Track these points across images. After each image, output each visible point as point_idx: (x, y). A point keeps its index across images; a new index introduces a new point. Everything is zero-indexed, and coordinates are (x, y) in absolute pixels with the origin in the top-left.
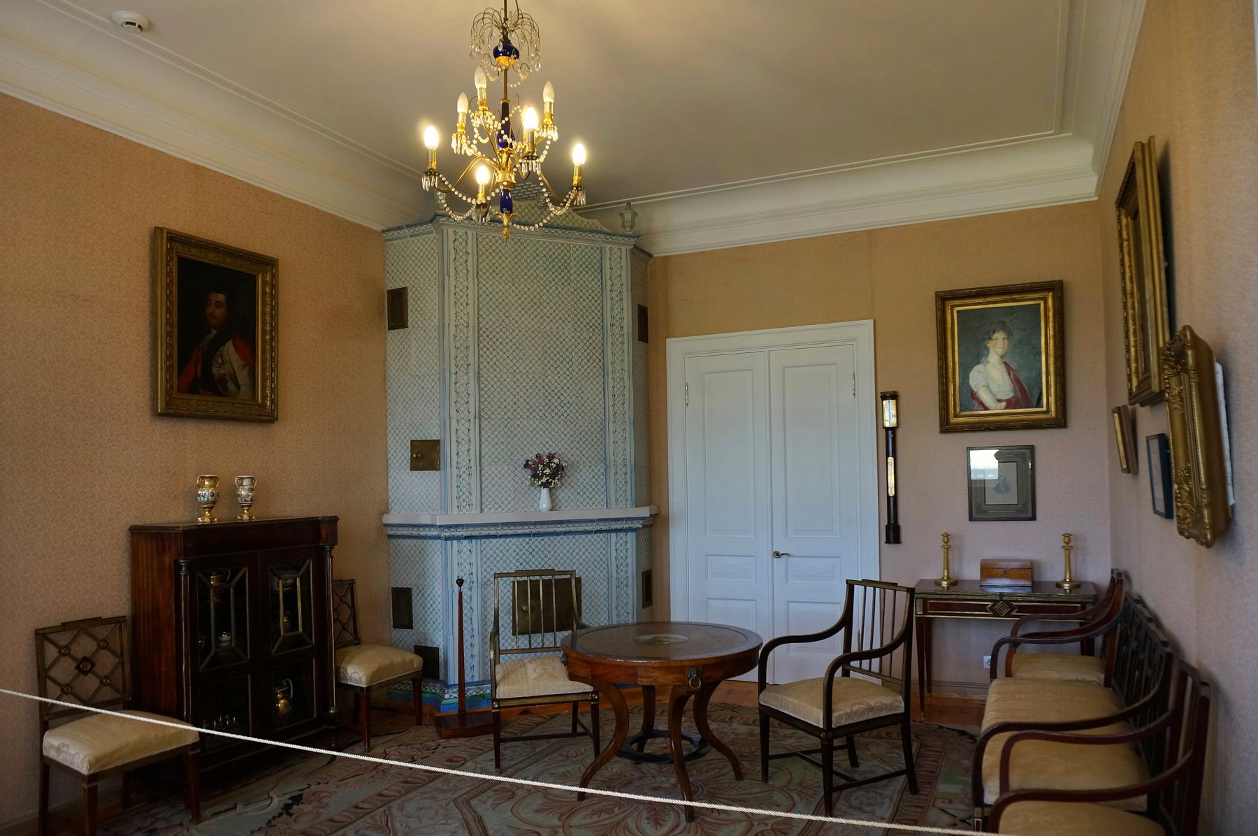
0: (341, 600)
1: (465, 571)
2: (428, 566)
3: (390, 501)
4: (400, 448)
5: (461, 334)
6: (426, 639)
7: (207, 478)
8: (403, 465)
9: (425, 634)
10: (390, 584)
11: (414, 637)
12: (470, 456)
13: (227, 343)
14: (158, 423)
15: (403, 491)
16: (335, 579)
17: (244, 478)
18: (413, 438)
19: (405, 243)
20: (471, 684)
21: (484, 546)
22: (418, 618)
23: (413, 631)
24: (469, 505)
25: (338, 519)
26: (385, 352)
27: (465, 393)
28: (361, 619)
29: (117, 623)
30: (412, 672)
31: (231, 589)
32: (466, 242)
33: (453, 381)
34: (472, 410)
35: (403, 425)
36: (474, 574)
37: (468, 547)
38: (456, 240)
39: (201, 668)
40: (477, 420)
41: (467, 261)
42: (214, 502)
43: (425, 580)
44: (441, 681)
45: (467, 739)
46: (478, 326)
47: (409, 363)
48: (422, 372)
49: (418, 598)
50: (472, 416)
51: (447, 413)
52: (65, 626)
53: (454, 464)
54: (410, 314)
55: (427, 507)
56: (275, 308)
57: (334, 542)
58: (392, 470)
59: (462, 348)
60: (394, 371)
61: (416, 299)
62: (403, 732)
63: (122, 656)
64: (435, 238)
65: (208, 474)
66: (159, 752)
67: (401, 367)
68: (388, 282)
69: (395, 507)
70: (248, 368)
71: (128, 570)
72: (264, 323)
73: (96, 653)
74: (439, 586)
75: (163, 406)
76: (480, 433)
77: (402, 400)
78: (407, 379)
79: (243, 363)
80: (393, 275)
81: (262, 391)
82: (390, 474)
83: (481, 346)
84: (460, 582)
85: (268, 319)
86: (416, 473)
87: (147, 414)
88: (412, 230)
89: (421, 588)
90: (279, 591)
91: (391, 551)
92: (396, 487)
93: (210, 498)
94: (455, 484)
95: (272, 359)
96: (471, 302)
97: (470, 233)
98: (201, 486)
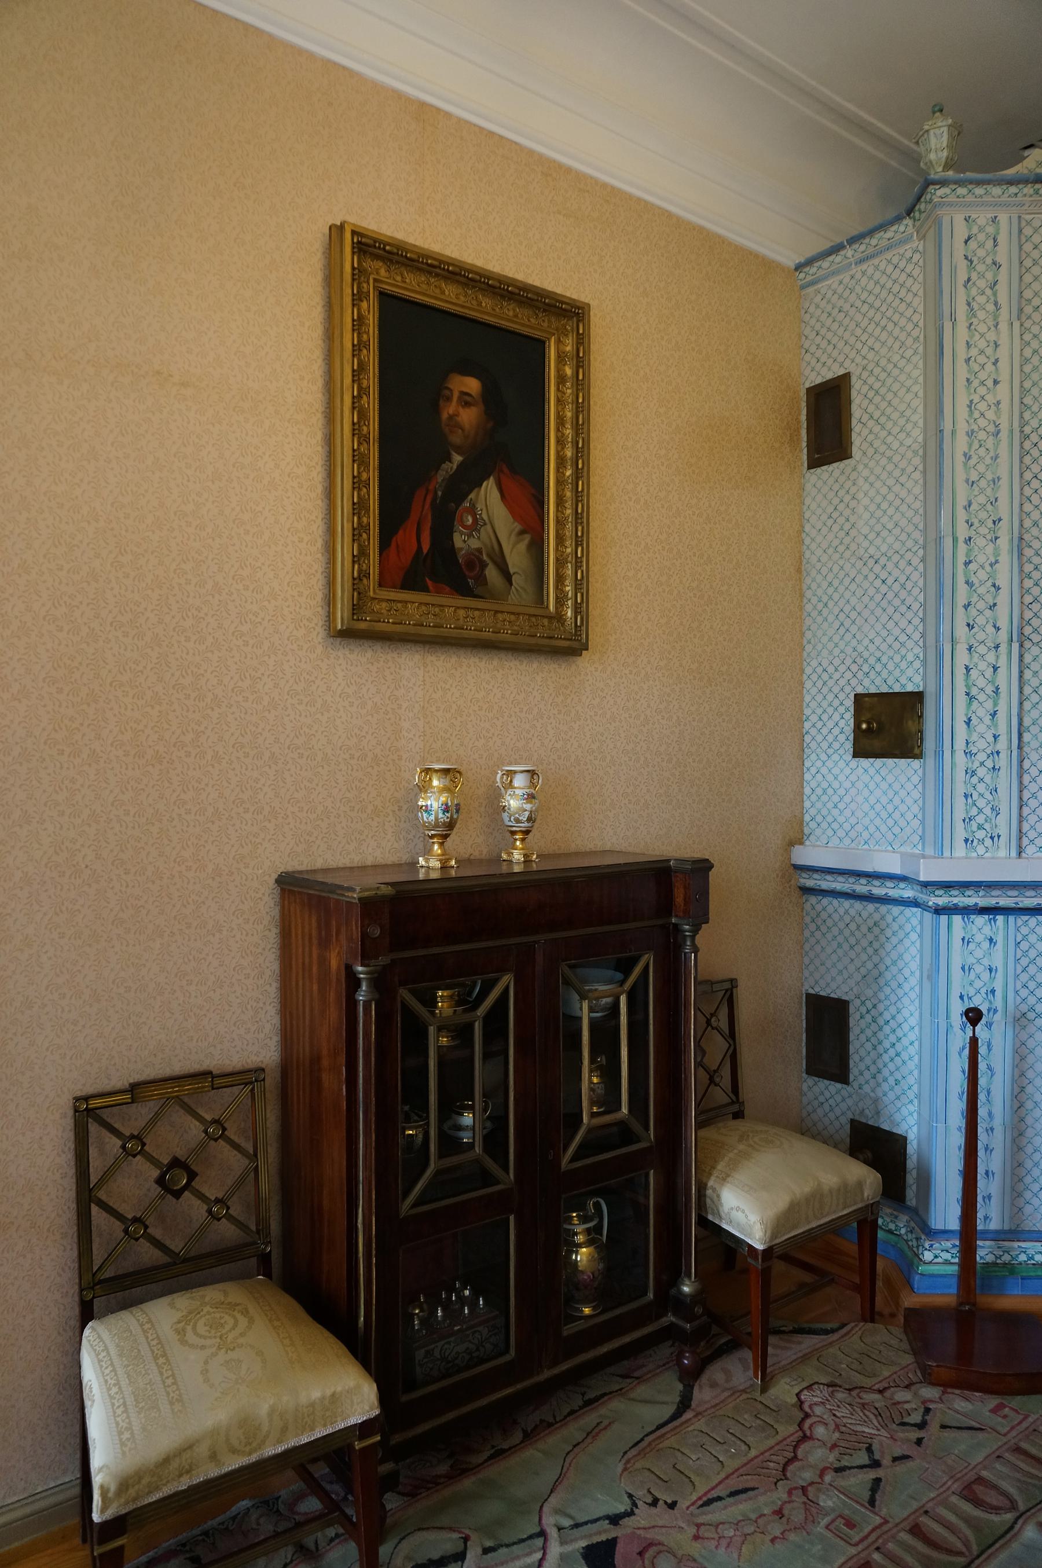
0: (708, 1022)
1: (978, 984)
2: (888, 962)
3: (807, 818)
4: (830, 710)
5: (982, 452)
6: (878, 1113)
7: (437, 771)
8: (836, 745)
9: (876, 1101)
10: (802, 985)
11: (850, 1102)
12: (996, 726)
13: (485, 484)
14: (340, 654)
15: (836, 799)
16: (699, 978)
17: (515, 772)
18: (860, 690)
19: (846, 280)
20: (987, 1235)
21: (1024, 930)
22: (862, 1066)
23: (849, 1089)
24: (992, 838)
25: (712, 866)
26: (801, 514)
27: (989, 583)
28: (746, 1058)
29: (246, 1084)
30: (860, 1205)
31: (477, 1024)
32: (995, 240)
33: (961, 559)
34: (1003, 623)
35: (837, 662)
36: (999, 994)
37: (987, 931)
38: (969, 238)
39: (406, 1207)
40: (1015, 646)
41: (996, 283)
42: (451, 825)
43: (880, 989)
44: (909, 1208)
45: (993, 1401)
46: (1022, 432)
47: (853, 532)
48: (884, 548)
49: (863, 1023)
50: (1003, 636)
51: (945, 628)
52: (136, 1091)
53: (960, 745)
54: (856, 427)
55: (890, 836)
56: (582, 408)
57: (701, 917)
58: (813, 757)
59: (983, 483)
60: (819, 552)
61: (871, 394)
62: (833, 1331)
63: (256, 1155)
64: (916, 251)
65: (438, 761)
66: (280, 1449)
67: (836, 542)
68: (807, 372)
69: (818, 832)
70: (527, 538)
71: (276, 966)
72: (560, 442)
73: (202, 1146)
74: (912, 1008)
75: (346, 615)
76: (1021, 673)
77: (836, 610)
78: (847, 567)
79: (518, 527)
80: (818, 354)
81: (557, 588)
82: (807, 764)
83: (1028, 476)
84: (973, 1016)
85: (568, 432)
86: (865, 762)
87: (318, 633)
88: (863, 247)
89: (869, 1005)
90: (580, 1019)
91: (808, 919)
92: (819, 791)
93: (441, 815)
94: (960, 789)
95: (578, 517)
96: (1004, 376)
97: (1003, 218)
98: (424, 787)
